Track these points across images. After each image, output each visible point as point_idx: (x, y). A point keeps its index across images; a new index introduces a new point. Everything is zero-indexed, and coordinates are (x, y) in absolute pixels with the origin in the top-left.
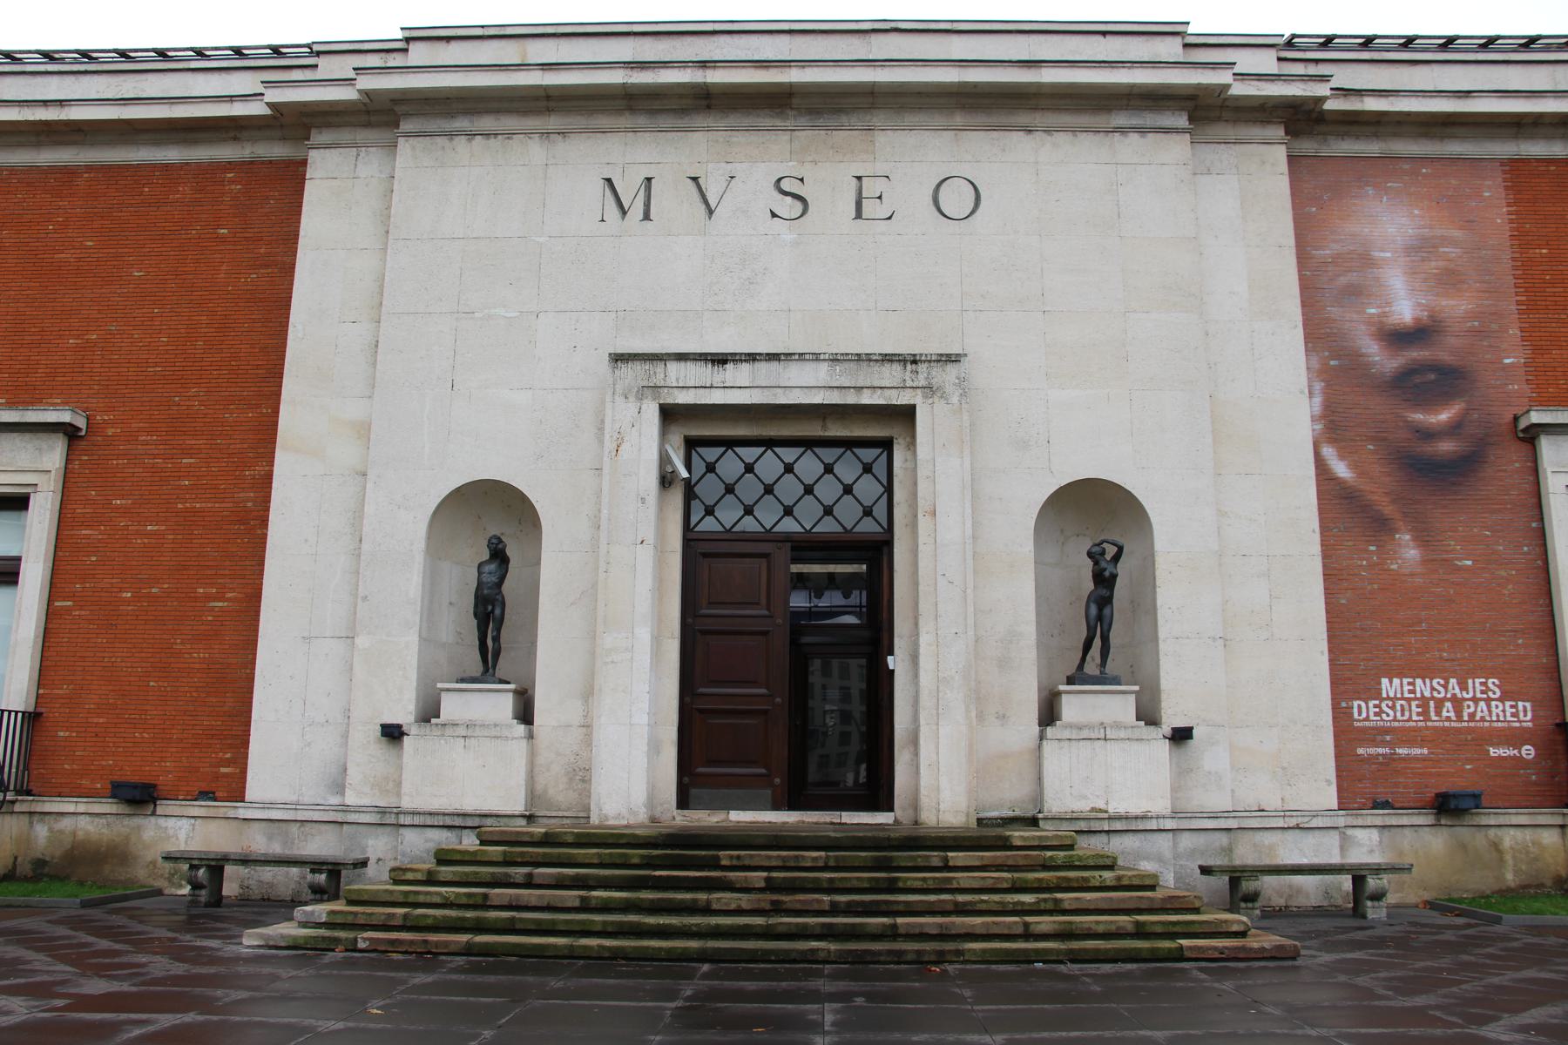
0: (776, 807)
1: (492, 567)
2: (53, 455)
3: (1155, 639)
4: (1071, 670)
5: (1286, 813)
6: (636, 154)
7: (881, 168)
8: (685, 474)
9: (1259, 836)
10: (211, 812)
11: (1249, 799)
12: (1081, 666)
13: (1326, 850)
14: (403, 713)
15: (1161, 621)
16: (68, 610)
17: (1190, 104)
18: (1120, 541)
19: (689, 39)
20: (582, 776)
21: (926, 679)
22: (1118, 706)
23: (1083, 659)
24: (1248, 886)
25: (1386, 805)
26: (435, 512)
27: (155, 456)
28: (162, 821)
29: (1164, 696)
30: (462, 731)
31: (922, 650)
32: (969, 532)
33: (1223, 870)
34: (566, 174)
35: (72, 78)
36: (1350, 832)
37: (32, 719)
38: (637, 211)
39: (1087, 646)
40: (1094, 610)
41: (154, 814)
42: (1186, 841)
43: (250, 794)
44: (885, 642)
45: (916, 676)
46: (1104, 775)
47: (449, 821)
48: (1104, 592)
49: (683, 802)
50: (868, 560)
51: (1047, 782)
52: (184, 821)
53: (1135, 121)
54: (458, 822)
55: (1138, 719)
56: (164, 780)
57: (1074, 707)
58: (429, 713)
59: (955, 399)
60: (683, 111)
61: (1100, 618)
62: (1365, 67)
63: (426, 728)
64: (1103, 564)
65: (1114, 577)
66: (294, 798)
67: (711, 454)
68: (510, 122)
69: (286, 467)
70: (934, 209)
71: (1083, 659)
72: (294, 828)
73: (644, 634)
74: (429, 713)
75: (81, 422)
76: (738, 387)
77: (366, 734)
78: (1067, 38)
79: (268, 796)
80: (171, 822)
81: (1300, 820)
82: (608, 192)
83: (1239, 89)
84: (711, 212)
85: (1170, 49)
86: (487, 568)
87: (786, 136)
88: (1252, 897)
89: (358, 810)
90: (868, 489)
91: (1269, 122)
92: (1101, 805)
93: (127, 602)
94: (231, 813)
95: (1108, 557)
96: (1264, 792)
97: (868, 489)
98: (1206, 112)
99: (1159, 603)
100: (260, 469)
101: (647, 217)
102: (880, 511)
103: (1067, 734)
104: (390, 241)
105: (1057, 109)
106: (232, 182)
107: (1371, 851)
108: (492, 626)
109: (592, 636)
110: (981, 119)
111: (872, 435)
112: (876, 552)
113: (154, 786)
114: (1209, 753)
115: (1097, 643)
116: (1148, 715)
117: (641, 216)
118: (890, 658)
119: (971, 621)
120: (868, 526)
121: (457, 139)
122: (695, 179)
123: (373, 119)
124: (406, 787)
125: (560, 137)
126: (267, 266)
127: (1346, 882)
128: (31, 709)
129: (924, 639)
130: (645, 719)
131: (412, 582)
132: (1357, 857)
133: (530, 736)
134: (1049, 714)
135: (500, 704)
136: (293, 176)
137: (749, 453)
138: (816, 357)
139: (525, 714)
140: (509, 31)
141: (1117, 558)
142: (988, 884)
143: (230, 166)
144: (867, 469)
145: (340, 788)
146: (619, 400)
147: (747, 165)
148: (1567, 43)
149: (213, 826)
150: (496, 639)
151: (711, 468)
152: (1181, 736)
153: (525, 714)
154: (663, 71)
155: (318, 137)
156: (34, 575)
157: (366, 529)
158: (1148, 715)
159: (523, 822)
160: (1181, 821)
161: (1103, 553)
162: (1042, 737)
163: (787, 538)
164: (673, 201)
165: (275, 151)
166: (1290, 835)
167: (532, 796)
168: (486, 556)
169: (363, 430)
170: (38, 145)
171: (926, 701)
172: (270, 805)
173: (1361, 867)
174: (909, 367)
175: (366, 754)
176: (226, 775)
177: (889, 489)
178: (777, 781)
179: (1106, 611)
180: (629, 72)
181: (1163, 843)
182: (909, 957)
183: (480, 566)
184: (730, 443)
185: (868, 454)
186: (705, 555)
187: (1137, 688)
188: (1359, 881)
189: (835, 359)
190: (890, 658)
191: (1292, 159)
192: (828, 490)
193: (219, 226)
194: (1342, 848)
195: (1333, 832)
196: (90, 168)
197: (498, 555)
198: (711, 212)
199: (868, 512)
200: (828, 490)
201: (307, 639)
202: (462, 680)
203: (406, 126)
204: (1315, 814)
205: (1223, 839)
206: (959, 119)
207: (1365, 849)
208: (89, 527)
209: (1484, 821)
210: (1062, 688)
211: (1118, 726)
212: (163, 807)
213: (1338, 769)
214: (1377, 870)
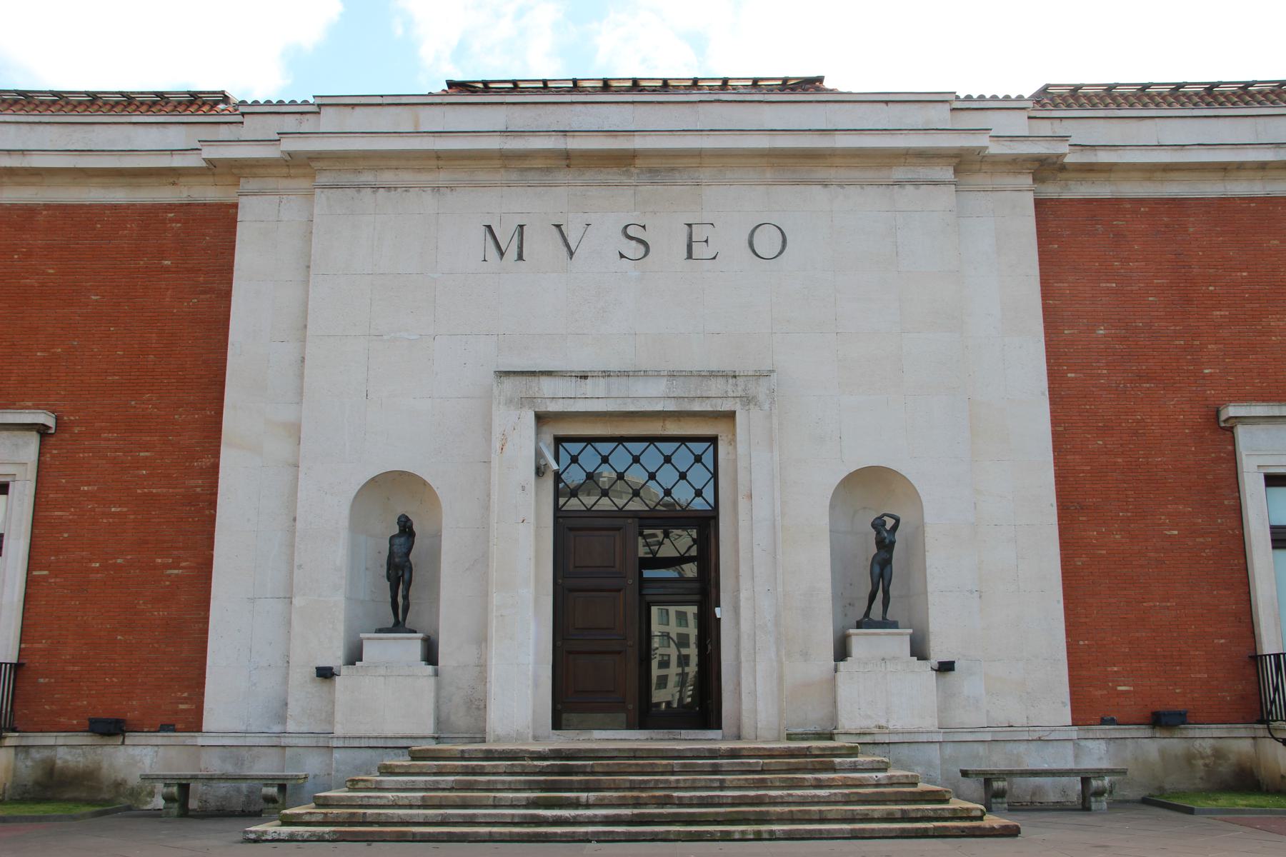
0: (629, 727)
1: (402, 540)
2: (29, 448)
3: (925, 593)
4: (860, 615)
6: (512, 204)
8: (555, 467)
12: (867, 614)
14: (334, 658)
16: (45, 578)
17: (957, 160)
20: (478, 706)
21: (745, 626)
22: (896, 643)
24: (997, 785)
25: (1112, 722)
26: (356, 497)
28: (131, 750)
30: (382, 671)
33: (978, 774)
34: (453, 223)
35: (27, 127)
36: (1083, 743)
37: (17, 667)
38: (512, 253)
39: (872, 598)
40: (877, 570)
41: (123, 743)
42: (949, 750)
44: (713, 596)
45: (738, 623)
46: (883, 696)
47: (373, 743)
48: (885, 555)
49: (557, 725)
52: (149, 748)
54: (381, 743)
55: (912, 655)
58: (354, 656)
59: (766, 407)
61: (882, 575)
65: (892, 543)
66: (243, 728)
67: (574, 448)
68: (407, 177)
69: (229, 460)
70: (749, 251)
72: (244, 752)
73: (527, 593)
74: (354, 656)
76: (595, 398)
77: (302, 674)
80: (137, 751)
81: (1041, 734)
82: (489, 237)
83: (995, 149)
84: (571, 254)
85: (939, 116)
86: (397, 541)
87: (630, 191)
88: (1001, 794)
90: (699, 476)
93: (97, 570)
94: (189, 741)
95: (888, 527)
96: (1010, 711)
98: (964, 163)
99: (928, 564)
100: (207, 462)
101: (520, 257)
102: (708, 493)
104: (312, 276)
107: (1100, 759)
108: (401, 575)
111: (699, 436)
112: (705, 525)
113: (123, 721)
114: (966, 683)
115: (880, 594)
116: (919, 650)
117: (516, 257)
118: (717, 610)
120: (698, 504)
121: (364, 191)
122: (558, 226)
123: (292, 171)
124: (338, 717)
126: (205, 292)
127: (1076, 784)
128: (15, 661)
129: (744, 595)
132: (1089, 763)
133: (436, 674)
134: (842, 652)
135: (411, 647)
138: (657, 374)
139: (430, 656)
140: (404, 100)
141: (895, 528)
143: (170, 207)
144: (698, 459)
145: (283, 719)
147: (602, 213)
149: (173, 752)
150: (406, 597)
151: (574, 460)
152: (946, 667)
153: (430, 656)
154: (531, 139)
155: (249, 184)
156: (18, 547)
157: (300, 512)
158: (919, 650)
159: (434, 742)
160: (949, 735)
162: (836, 670)
163: (635, 515)
164: (541, 244)
165: (209, 193)
166: (1033, 746)
168: (396, 530)
169: (295, 431)
171: (745, 643)
172: (225, 733)
173: (1086, 771)
174: (731, 381)
176: (182, 710)
177: (715, 475)
178: (631, 707)
179: (887, 571)
180: (503, 139)
181: (934, 753)
182: (737, 836)
183: (392, 538)
184: (590, 440)
185: (698, 448)
186: (571, 529)
187: (911, 631)
188: (1085, 781)
189: (672, 375)
190: (717, 610)
191: (1039, 204)
192: (667, 476)
194: (1076, 757)
195: (1067, 743)
198: (571, 254)
199: (699, 493)
200: (667, 476)
201: (252, 600)
203: (323, 179)
204: (1053, 729)
206: (769, 175)
208: (61, 509)
209: (1191, 734)
210: (362, 635)
212: (131, 739)
213: (1072, 693)
214: (1100, 773)
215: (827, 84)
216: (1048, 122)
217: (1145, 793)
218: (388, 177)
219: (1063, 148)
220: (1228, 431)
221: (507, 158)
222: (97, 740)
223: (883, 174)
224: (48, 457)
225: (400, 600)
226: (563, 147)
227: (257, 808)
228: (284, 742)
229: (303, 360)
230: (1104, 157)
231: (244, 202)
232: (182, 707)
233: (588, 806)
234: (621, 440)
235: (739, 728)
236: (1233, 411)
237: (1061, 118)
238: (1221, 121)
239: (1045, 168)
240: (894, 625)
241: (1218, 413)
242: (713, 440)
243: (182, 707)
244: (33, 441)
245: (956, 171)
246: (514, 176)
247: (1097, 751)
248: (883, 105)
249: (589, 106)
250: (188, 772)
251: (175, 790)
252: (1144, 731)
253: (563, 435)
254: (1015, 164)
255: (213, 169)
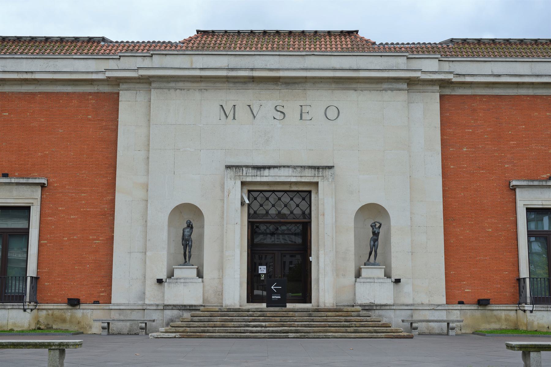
3: (391, 252)
5: (430, 305)
7: (308, 103)
9: (422, 312)
10: (98, 307)
11: (418, 301)
13: (443, 315)
14: (163, 276)
15: (392, 247)
16: (46, 244)
17: (408, 81)
18: (381, 222)
19: (246, 57)
22: (379, 272)
23: (369, 257)
24: (414, 325)
27: (72, 193)
29: (392, 269)
30: (182, 281)
31: (320, 256)
32: (334, 220)
38: (231, 116)
43: (113, 301)
46: (373, 290)
48: (375, 237)
50: (304, 227)
51: (357, 294)
53: (390, 86)
56: (82, 298)
57: (365, 272)
58: (171, 275)
59: (330, 180)
60: (245, 83)
61: (374, 245)
62: (469, 63)
63: (170, 280)
64: (375, 229)
65: (379, 233)
66: (127, 302)
68: (188, 85)
71: (369, 257)
73: (238, 252)
74: (171, 275)
75: (46, 183)
76: (267, 176)
77: (151, 282)
78: (369, 57)
79: (119, 302)
84: (254, 117)
89: (150, 305)
91: (434, 85)
92: (373, 302)
93: (66, 241)
95: (377, 226)
97: (304, 205)
101: (234, 118)
103: (365, 280)
105: (365, 83)
106: (91, 99)
108: (188, 244)
109: (222, 251)
110: (341, 86)
111: (305, 194)
114: (406, 287)
116: (388, 275)
119: (334, 247)
121: (171, 90)
122: (249, 106)
123: (141, 81)
125: (205, 91)
126: (106, 129)
127: (446, 324)
130: (239, 276)
131: (164, 235)
133: (203, 282)
134: (358, 275)
135: (191, 272)
136: (115, 99)
137: (267, 194)
139: (200, 275)
141: (380, 227)
142: (337, 320)
146: (229, 180)
148: (550, 42)
150: (190, 252)
152: (398, 281)
153: (200, 275)
155: (122, 86)
157: (149, 218)
158: (388, 275)
161: (375, 226)
162: (356, 282)
164: (242, 113)
165: (106, 89)
166: (431, 312)
167: (204, 301)
168: (186, 226)
169: (146, 187)
170: (21, 85)
171: (321, 271)
172: (118, 305)
175: (151, 289)
176: (102, 296)
177: (310, 206)
179: (376, 243)
185: (304, 195)
188: (448, 324)
191: (442, 97)
192: (293, 205)
193: (89, 115)
196: (40, 93)
197: (190, 226)
198: (254, 117)
202: (180, 265)
203: (153, 85)
205: (409, 312)
206: (333, 86)
207: (455, 316)
210: (362, 267)
211: (379, 278)
212: (82, 306)
214: (453, 322)
215: (360, 34)
216: (447, 62)
217: (473, 330)
218: (181, 85)
219: (450, 77)
220: (513, 189)
221: (227, 79)
222: (70, 307)
223: (379, 86)
224: (45, 196)
225: (187, 253)
226: (251, 75)
227: (136, 332)
228: (145, 307)
229: (148, 158)
230: (468, 79)
231: (121, 92)
232: (101, 294)
233: (265, 327)
234: (274, 191)
235: (318, 303)
236: (514, 183)
237: (453, 61)
238: (517, 63)
239: (444, 84)
240: (378, 265)
241: (510, 182)
242: (310, 192)
243: (101, 294)
244: (39, 189)
245: (408, 84)
246: (231, 85)
247: (456, 314)
248: (380, 57)
249: (261, 56)
250: (109, 319)
251: (106, 325)
252: (475, 307)
253: (255, 194)
254: (432, 82)
255: (109, 81)
